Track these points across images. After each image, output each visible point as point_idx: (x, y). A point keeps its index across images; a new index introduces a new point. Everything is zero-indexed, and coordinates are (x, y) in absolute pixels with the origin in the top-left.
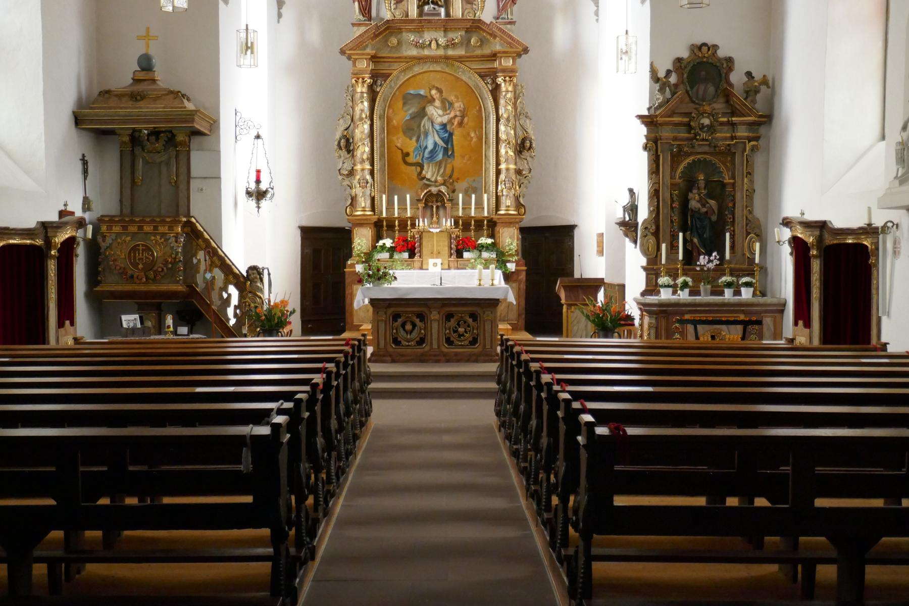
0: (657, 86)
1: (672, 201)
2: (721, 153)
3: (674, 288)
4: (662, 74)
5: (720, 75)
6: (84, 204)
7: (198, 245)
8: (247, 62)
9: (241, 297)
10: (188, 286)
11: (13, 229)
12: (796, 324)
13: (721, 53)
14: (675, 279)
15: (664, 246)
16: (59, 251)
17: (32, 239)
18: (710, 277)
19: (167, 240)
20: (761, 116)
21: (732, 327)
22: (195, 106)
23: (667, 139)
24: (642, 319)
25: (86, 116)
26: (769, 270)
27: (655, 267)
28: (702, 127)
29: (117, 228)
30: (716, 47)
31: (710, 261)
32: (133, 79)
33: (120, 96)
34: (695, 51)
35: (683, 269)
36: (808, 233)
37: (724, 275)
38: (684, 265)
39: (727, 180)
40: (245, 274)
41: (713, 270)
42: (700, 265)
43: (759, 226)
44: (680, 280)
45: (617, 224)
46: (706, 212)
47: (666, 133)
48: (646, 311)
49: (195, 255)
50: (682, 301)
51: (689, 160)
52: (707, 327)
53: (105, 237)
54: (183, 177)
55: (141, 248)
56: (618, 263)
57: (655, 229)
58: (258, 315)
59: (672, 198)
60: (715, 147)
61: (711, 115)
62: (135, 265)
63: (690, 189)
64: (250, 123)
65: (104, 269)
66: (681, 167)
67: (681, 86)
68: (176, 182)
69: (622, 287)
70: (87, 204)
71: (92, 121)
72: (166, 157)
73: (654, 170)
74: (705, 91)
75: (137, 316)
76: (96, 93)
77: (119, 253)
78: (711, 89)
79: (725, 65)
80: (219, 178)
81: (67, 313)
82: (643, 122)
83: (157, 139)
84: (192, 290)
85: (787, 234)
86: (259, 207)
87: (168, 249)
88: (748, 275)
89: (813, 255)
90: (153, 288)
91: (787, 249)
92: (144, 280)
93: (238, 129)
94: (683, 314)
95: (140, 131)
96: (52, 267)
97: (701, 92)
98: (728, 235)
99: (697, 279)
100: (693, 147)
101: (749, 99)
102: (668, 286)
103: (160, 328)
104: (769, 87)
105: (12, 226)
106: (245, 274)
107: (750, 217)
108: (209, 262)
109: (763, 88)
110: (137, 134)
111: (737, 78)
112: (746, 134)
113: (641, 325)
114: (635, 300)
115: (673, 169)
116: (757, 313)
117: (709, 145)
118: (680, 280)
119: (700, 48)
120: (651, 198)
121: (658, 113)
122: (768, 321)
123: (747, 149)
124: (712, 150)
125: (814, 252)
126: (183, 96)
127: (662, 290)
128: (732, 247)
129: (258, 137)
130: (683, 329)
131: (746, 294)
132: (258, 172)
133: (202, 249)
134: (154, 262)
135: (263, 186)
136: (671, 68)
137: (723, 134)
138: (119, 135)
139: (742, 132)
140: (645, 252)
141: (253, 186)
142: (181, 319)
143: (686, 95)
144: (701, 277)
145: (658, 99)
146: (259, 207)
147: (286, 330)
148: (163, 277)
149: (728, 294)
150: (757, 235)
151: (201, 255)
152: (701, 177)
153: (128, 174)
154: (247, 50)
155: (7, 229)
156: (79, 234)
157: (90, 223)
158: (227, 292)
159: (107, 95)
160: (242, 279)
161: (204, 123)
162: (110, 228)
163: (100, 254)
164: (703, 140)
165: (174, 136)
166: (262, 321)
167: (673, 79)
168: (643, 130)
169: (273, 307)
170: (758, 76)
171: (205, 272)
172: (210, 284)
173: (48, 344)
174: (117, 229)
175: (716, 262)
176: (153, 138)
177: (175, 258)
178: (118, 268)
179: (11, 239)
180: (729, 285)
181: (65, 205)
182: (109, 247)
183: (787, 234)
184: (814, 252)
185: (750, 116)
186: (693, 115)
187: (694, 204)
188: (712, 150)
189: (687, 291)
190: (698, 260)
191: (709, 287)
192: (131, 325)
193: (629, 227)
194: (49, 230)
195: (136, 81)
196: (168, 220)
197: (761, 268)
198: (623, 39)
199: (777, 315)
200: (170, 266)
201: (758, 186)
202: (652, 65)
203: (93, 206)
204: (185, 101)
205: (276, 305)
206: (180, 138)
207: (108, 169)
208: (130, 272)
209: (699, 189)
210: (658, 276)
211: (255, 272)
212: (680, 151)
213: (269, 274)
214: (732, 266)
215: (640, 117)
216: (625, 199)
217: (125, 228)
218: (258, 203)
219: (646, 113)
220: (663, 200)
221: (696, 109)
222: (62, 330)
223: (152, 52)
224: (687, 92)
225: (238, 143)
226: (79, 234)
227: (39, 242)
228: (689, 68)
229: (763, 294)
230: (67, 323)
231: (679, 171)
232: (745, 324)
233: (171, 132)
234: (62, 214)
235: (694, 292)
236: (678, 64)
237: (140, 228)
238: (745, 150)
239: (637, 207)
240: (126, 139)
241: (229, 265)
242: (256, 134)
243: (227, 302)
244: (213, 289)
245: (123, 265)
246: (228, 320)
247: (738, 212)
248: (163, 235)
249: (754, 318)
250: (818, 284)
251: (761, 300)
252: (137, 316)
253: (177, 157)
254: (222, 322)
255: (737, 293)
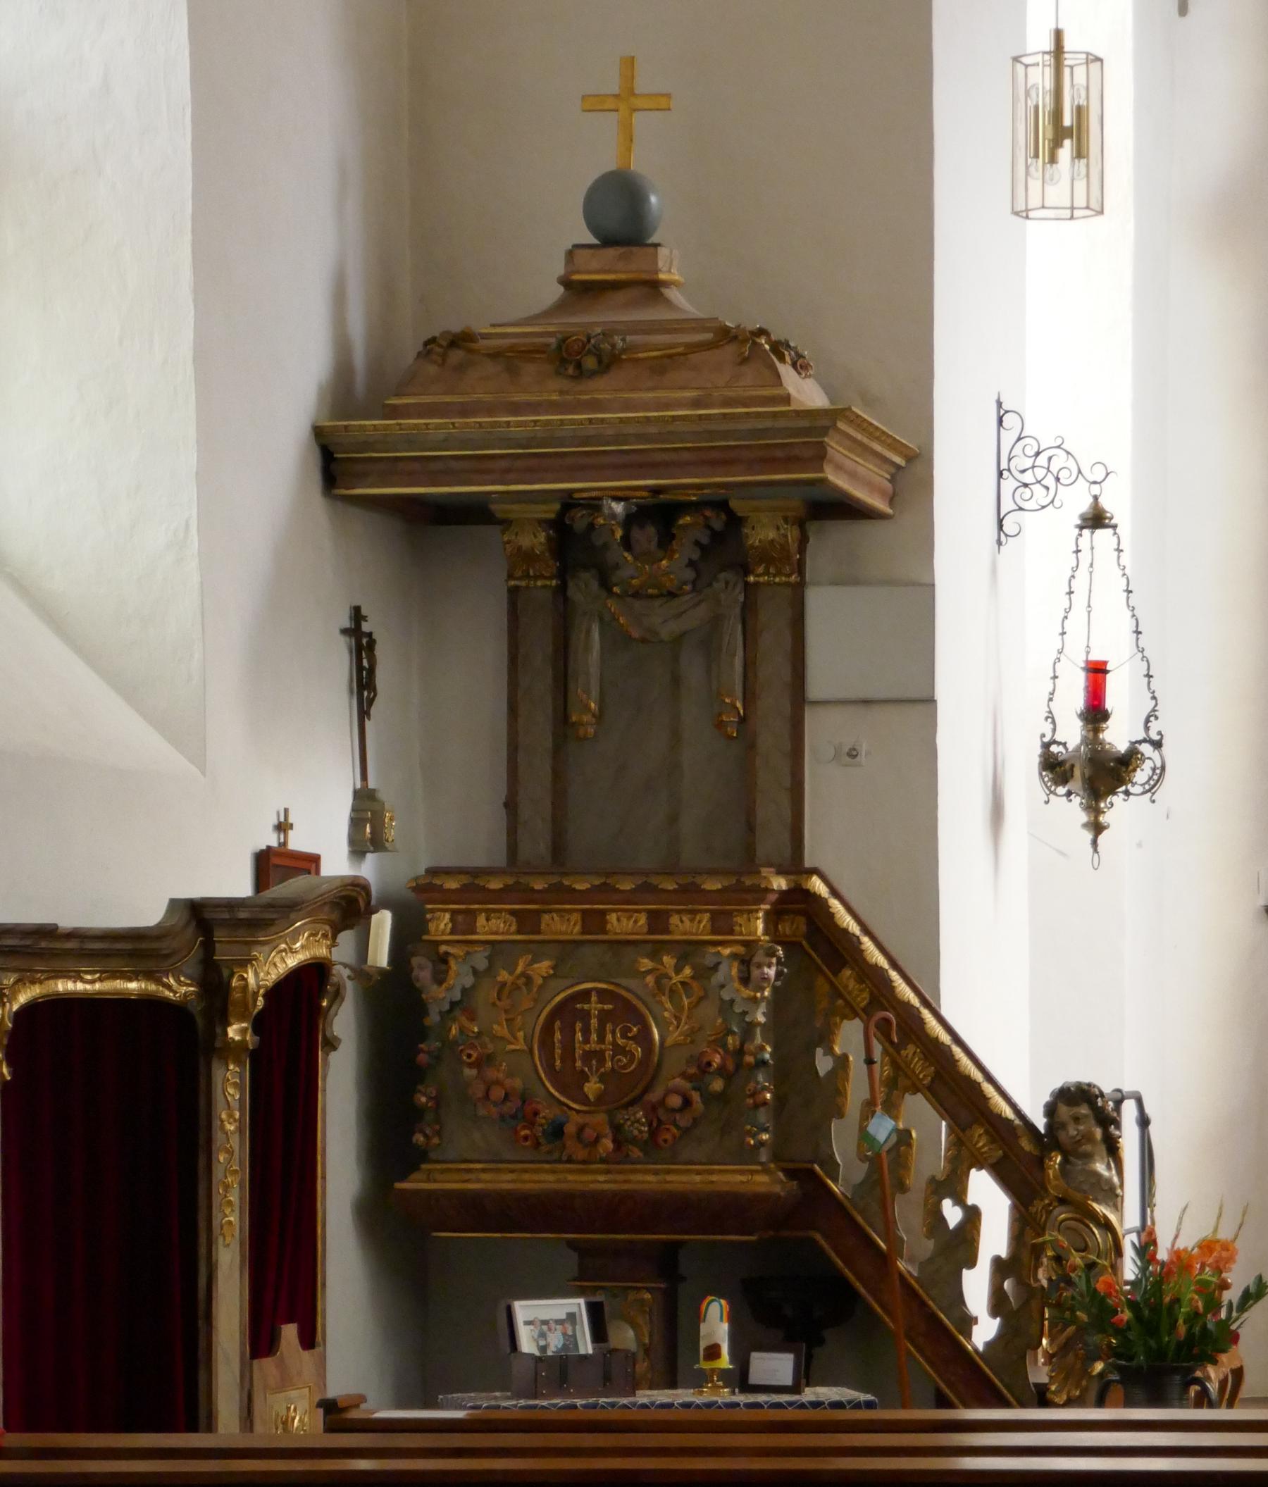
6: (356, 823)
7: (837, 993)
8: (1058, 194)
9: (1025, 1224)
10: (791, 1174)
11: (74, 934)
16: (259, 1025)
17: (149, 975)
19: (704, 973)
22: (828, 389)
25: (367, 445)
29: (497, 924)
32: (566, 282)
33: (512, 357)
40: (1040, 1122)
49: (825, 1039)
53: (444, 959)
54: (773, 702)
55: (594, 1006)
58: (1102, 1309)
62: (571, 1083)
64: (1060, 461)
65: (438, 1100)
68: (743, 720)
70: (368, 826)
71: (393, 469)
72: (696, 617)
75: (578, 1305)
76: (410, 346)
77: (501, 1030)
80: (930, 701)
81: (286, 1294)
83: (666, 540)
84: (809, 1180)
86: (1097, 828)
87: (709, 1010)
90: (647, 1179)
92: (608, 1144)
93: (1008, 485)
95: (594, 505)
96: (230, 1090)
103: (674, 1356)
105: (67, 921)
106: (1040, 1122)
108: (882, 1070)
110: (579, 520)
126: (779, 348)
129: (1096, 519)
132: (1097, 672)
133: (852, 1012)
134: (650, 1071)
135: (1118, 736)
138: (506, 523)
141: (1072, 734)
142: (763, 1321)
146: (1097, 828)
147: (1214, 1375)
148: (686, 1131)
151: (850, 1037)
153: (540, 685)
154: (1056, 143)
155: (47, 932)
156: (342, 951)
157: (385, 904)
158: (829, 1051)
159: (456, 356)
160: (1026, 1144)
161: (867, 468)
162: (463, 922)
163: (423, 1034)
165: (735, 522)
166: (1119, 1331)
169: (1167, 1271)
171: (868, 1109)
172: (887, 1167)
173: (210, 1428)
174: (494, 926)
176: (647, 536)
177: (740, 1052)
178: (498, 1093)
179: (65, 975)
181: (283, 827)
182: (462, 1005)
192: (555, 1342)
194: (220, 935)
195: (580, 291)
196: (713, 885)
200: (717, 1085)
203: (392, 832)
204: (786, 371)
205: (1181, 1261)
206: (763, 532)
207: (463, 669)
208: (547, 1113)
211: (1086, 1114)
213: (1144, 1122)
217: (528, 922)
218: (1094, 809)
222: (267, 1365)
223: (642, 164)
225: (1010, 545)
226: (342, 951)
227: (178, 988)
230: (290, 1332)
233: (722, 506)
234: (268, 865)
237: (593, 921)
240: (536, 540)
241: (968, 1079)
242: (1085, 505)
243: (962, 1245)
244: (902, 1187)
245: (518, 1083)
246: (967, 1322)
248: (688, 950)
252: (578, 1305)
253: (748, 611)
254: (941, 1327)
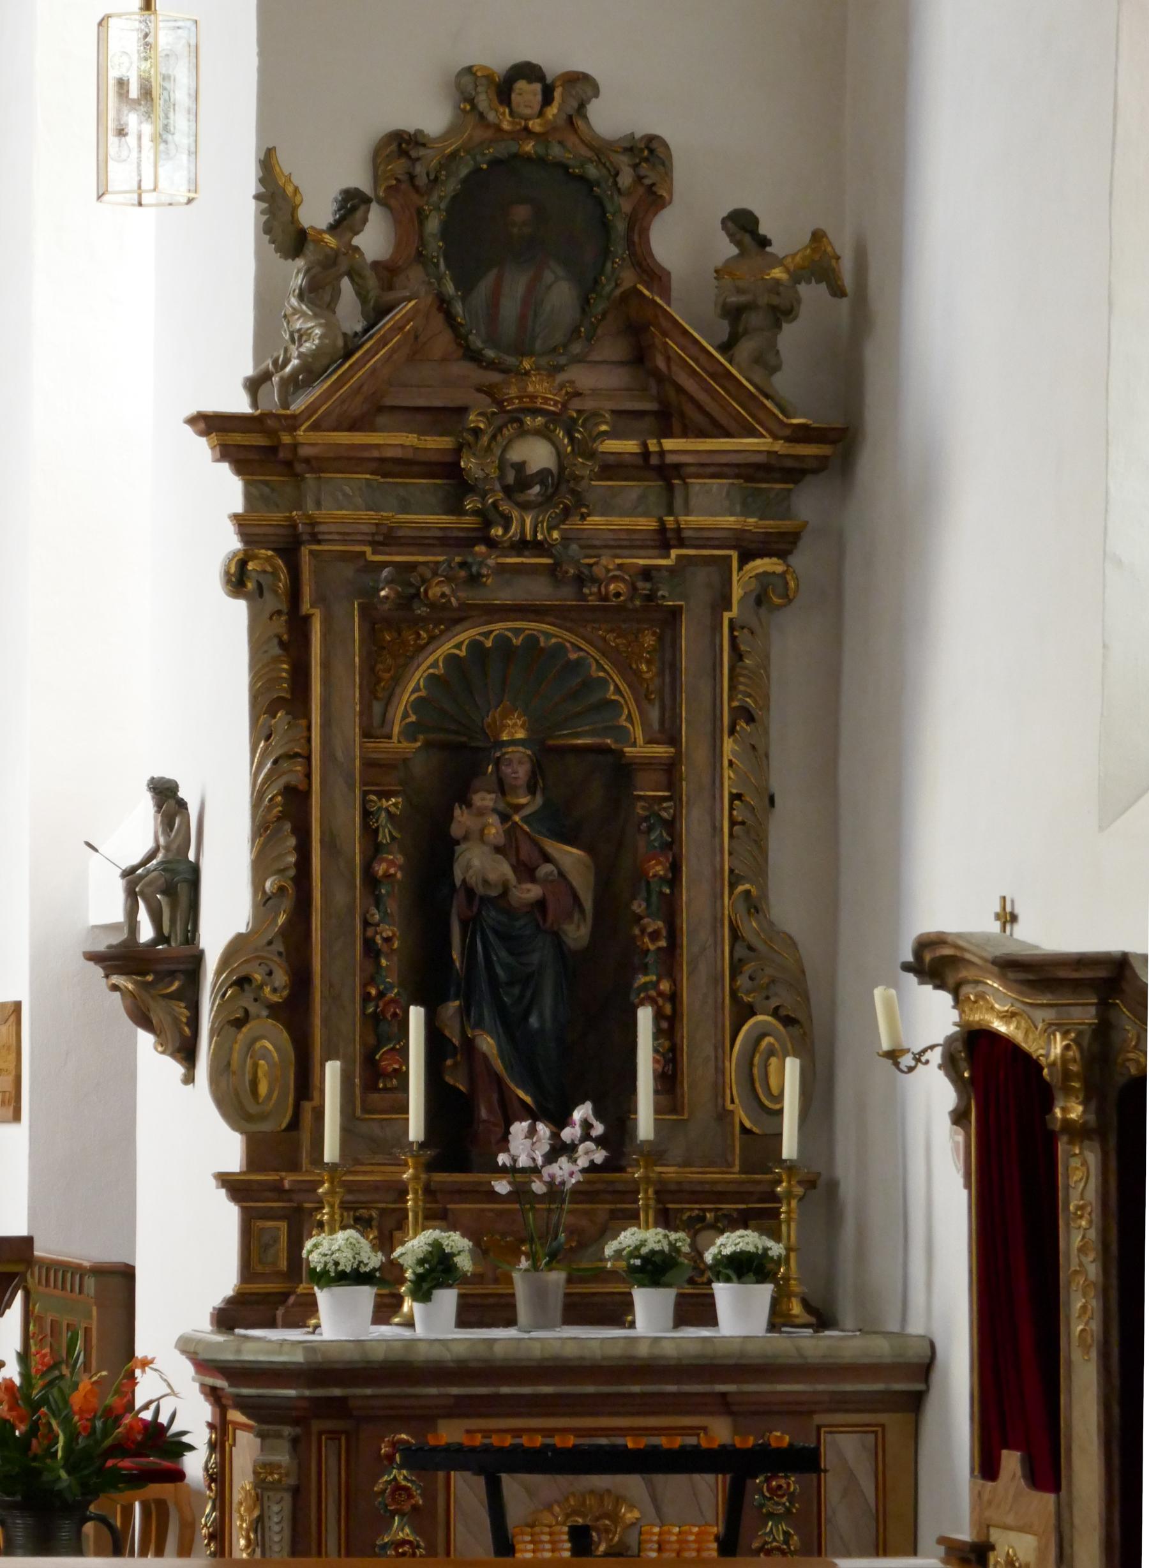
0: (295, 273)
1: (374, 850)
2: (610, 612)
3: (387, 1289)
4: (317, 213)
5: (605, 227)
12: (987, 1467)
13: (609, 118)
14: (386, 1242)
15: (332, 1072)
18: (560, 1232)
20: (803, 434)
21: (673, 1485)
23: (345, 537)
24: (220, 1445)
26: (848, 1190)
27: (288, 1180)
28: (520, 481)
30: (581, 84)
31: (560, 1149)
34: (483, 102)
35: (429, 1192)
36: (1042, 1016)
37: (631, 1218)
38: (432, 1166)
39: (640, 747)
41: (578, 1193)
42: (511, 1170)
43: (798, 981)
44: (414, 1246)
45: (94, 957)
46: (541, 905)
47: (341, 509)
48: (243, 1405)
50: (423, 1353)
51: (456, 642)
52: (549, 1485)
56: (95, 1160)
57: (285, 980)
59: (370, 832)
60: (580, 580)
61: (561, 422)
63: (460, 792)
66: (415, 683)
67: (416, 274)
69: (119, 1282)
73: (282, 691)
74: (531, 302)
78: (561, 295)
79: (626, 179)
82: (226, 453)
85: (934, 1016)
88: (742, 1221)
89: (1067, 1124)
91: (934, 1095)
94: (425, 1417)
97: (510, 309)
98: (645, 1017)
99: (495, 1246)
100: (474, 580)
101: (746, 348)
102: (357, 1277)
104: (838, 291)
107: (750, 927)
109: (811, 294)
111: (683, 242)
112: (729, 521)
113: (219, 1476)
114: (188, 1347)
115: (377, 687)
116: (797, 1410)
117: (553, 572)
118: (414, 1246)
119: (502, 90)
120: (264, 830)
121: (299, 405)
122: (846, 1450)
123: (737, 593)
124: (565, 596)
125: (1071, 1110)
127: (323, 1297)
128: (668, 1081)
130: (429, 1495)
131: (740, 1314)
136: (359, 179)
137: (617, 517)
139: (711, 511)
140: (235, 1104)
143: (438, 320)
144: (520, 1227)
145: (299, 337)
149: (650, 1313)
150: (788, 1021)
152: (515, 730)
164: (522, 545)
167: (374, 239)
168: (228, 490)
170: (785, 234)
175: (591, 1154)
180: (654, 1269)
183: (934, 1016)
184: (1071, 1110)
185: (752, 433)
186: (473, 419)
187: (479, 863)
188: (565, 596)
189: (447, 1299)
190: (503, 1143)
191: (557, 1277)
193: (151, 973)
197: (811, 1184)
198: (124, 37)
199: (892, 1420)
201: (787, 775)
202: (268, 164)
209: (502, 788)
210: (301, 1223)
212: (408, 600)
214: (670, 1172)
215: (210, 424)
216: (136, 835)
219: (240, 404)
220: (331, 846)
221: (488, 391)
224: (443, 304)
228: (451, 187)
229: (822, 1318)
231: (406, 696)
232: (738, 1466)
235: (484, 1307)
236: (399, 166)
238: (725, 602)
239: (195, 872)
247: (694, 900)
249: (780, 1438)
250: (1093, 1270)
251: (809, 1344)
255: (696, 1309)
